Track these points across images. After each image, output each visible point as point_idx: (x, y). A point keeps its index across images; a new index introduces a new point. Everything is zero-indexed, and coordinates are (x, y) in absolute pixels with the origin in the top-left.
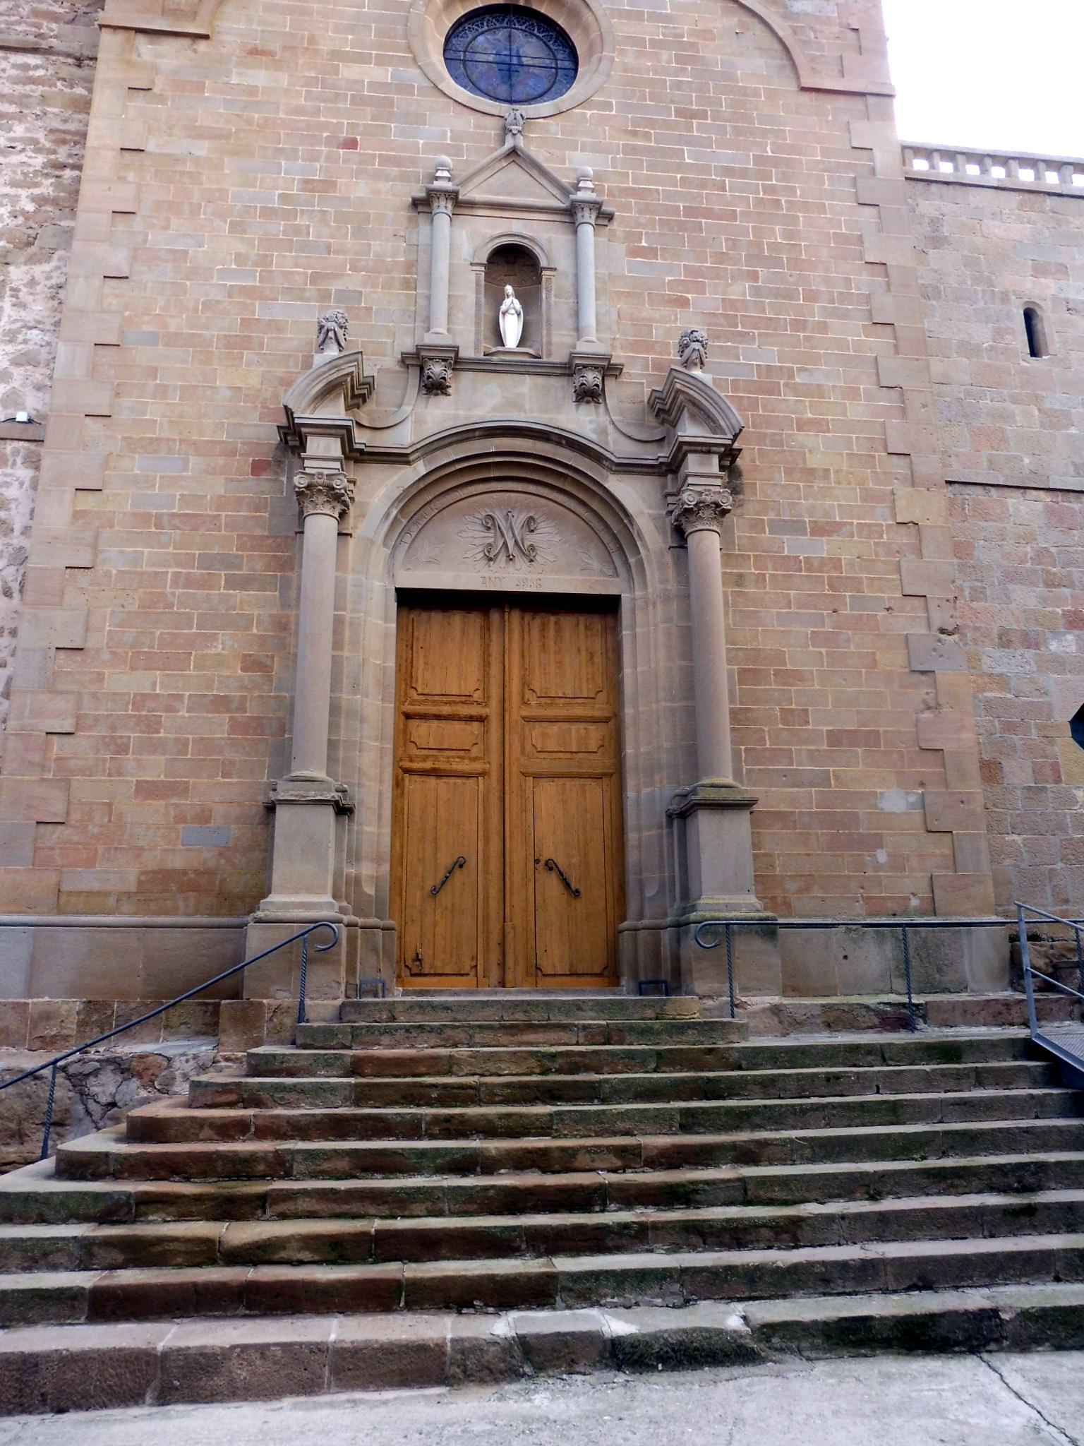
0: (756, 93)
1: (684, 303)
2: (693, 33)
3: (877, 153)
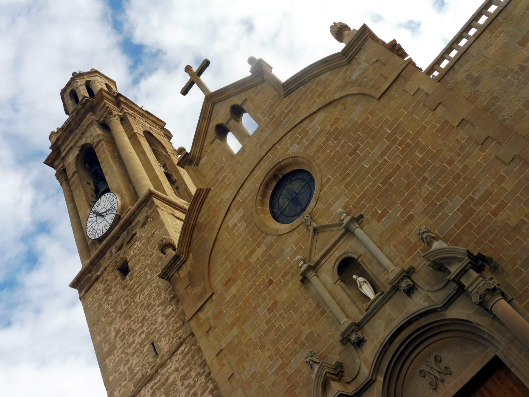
0: (367, 118)
1: (411, 217)
2: (332, 126)
3: (423, 87)
